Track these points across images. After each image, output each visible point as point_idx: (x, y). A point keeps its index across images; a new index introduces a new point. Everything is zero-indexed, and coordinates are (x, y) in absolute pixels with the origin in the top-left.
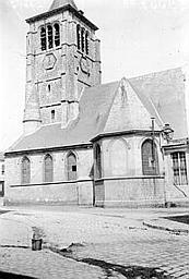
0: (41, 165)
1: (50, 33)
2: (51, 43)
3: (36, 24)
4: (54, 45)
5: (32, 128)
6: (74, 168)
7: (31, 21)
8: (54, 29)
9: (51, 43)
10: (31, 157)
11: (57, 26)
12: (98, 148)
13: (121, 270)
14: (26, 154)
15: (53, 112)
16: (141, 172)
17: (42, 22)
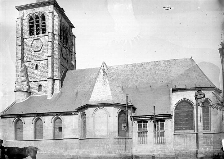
0: (32, 126)
1: (37, 22)
2: (38, 30)
3: (25, 11)
4: (41, 32)
5: (22, 98)
6: (60, 129)
7: (20, 9)
8: (41, 19)
9: (38, 30)
10: (24, 119)
11: (44, 18)
12: (84, 114)
13: (83, 157)
14: (19, 117)
15: (40, 86)
16: (117, 133)
17: (30, 11)
